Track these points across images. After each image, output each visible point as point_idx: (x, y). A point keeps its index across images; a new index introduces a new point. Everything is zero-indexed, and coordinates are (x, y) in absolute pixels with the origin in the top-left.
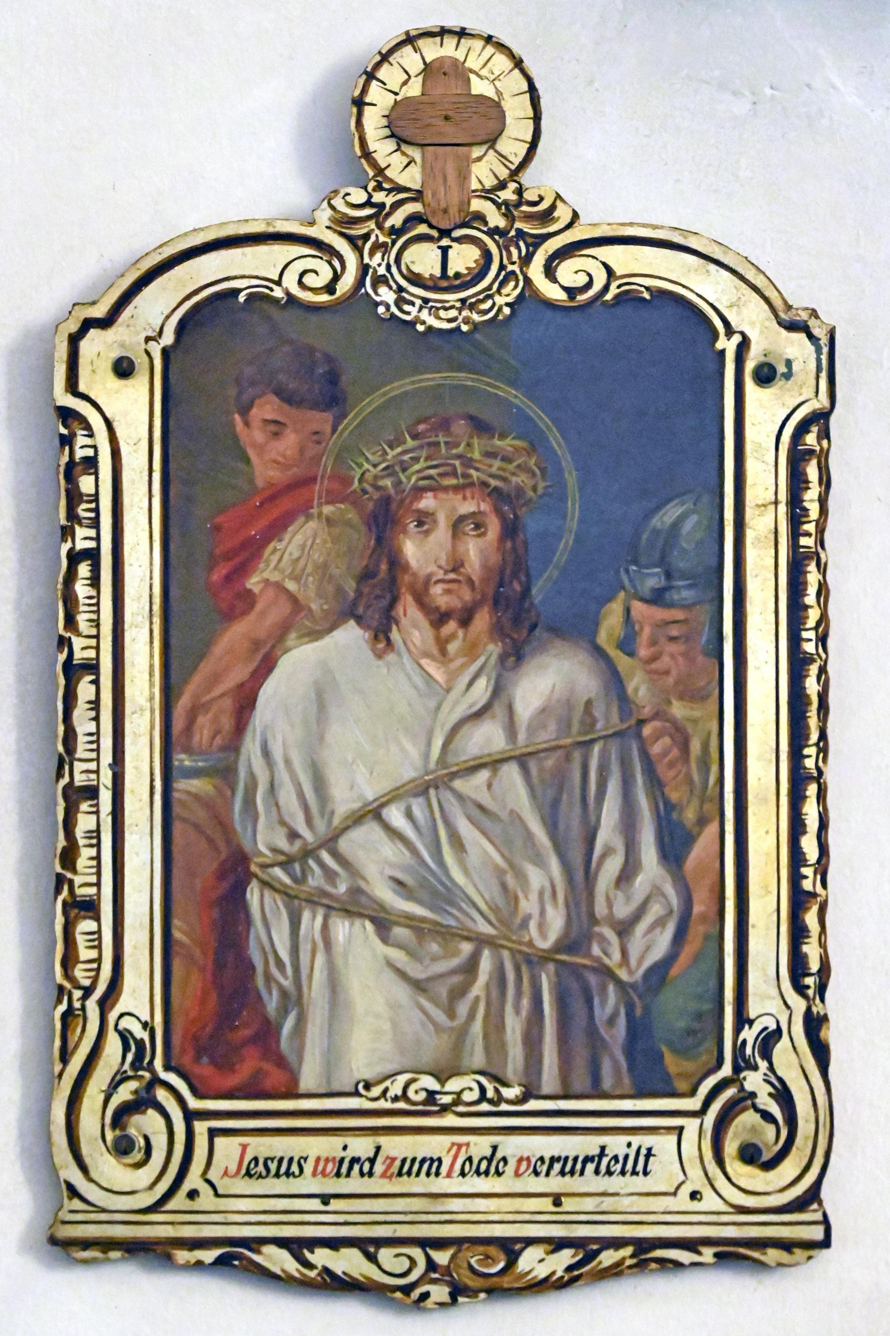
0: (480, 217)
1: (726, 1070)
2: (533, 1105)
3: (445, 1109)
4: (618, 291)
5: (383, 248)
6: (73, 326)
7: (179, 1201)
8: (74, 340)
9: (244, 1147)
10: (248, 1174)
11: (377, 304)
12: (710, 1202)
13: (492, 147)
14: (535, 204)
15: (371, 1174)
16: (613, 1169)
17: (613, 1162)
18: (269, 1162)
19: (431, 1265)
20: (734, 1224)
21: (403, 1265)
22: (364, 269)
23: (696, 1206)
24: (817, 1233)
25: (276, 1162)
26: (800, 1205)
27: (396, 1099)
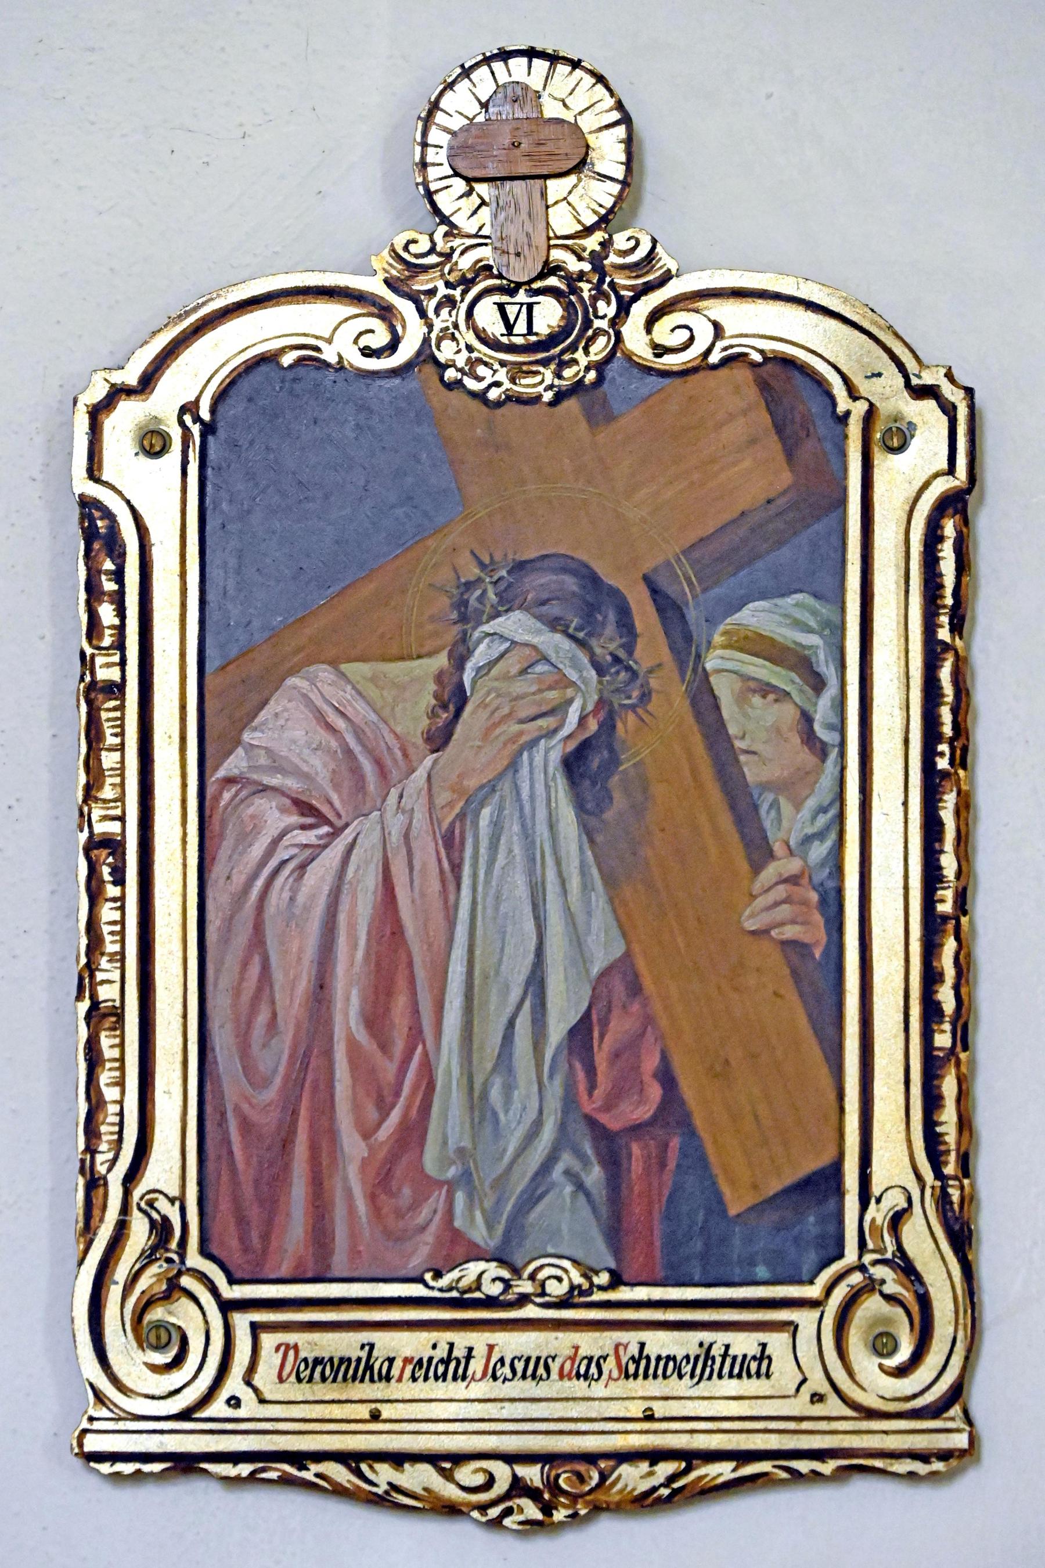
2: (624, 1294)
3: (523, 1300)
5: (450, 302)
6: (97, 392)
7: (218, 1408)
9: (491, 1348)
18: (516, 1361)
19: (516, 1479)
20: (641, 1432)
21: (480, 1479)
23: (818, 1410)
24: (961, 1441)
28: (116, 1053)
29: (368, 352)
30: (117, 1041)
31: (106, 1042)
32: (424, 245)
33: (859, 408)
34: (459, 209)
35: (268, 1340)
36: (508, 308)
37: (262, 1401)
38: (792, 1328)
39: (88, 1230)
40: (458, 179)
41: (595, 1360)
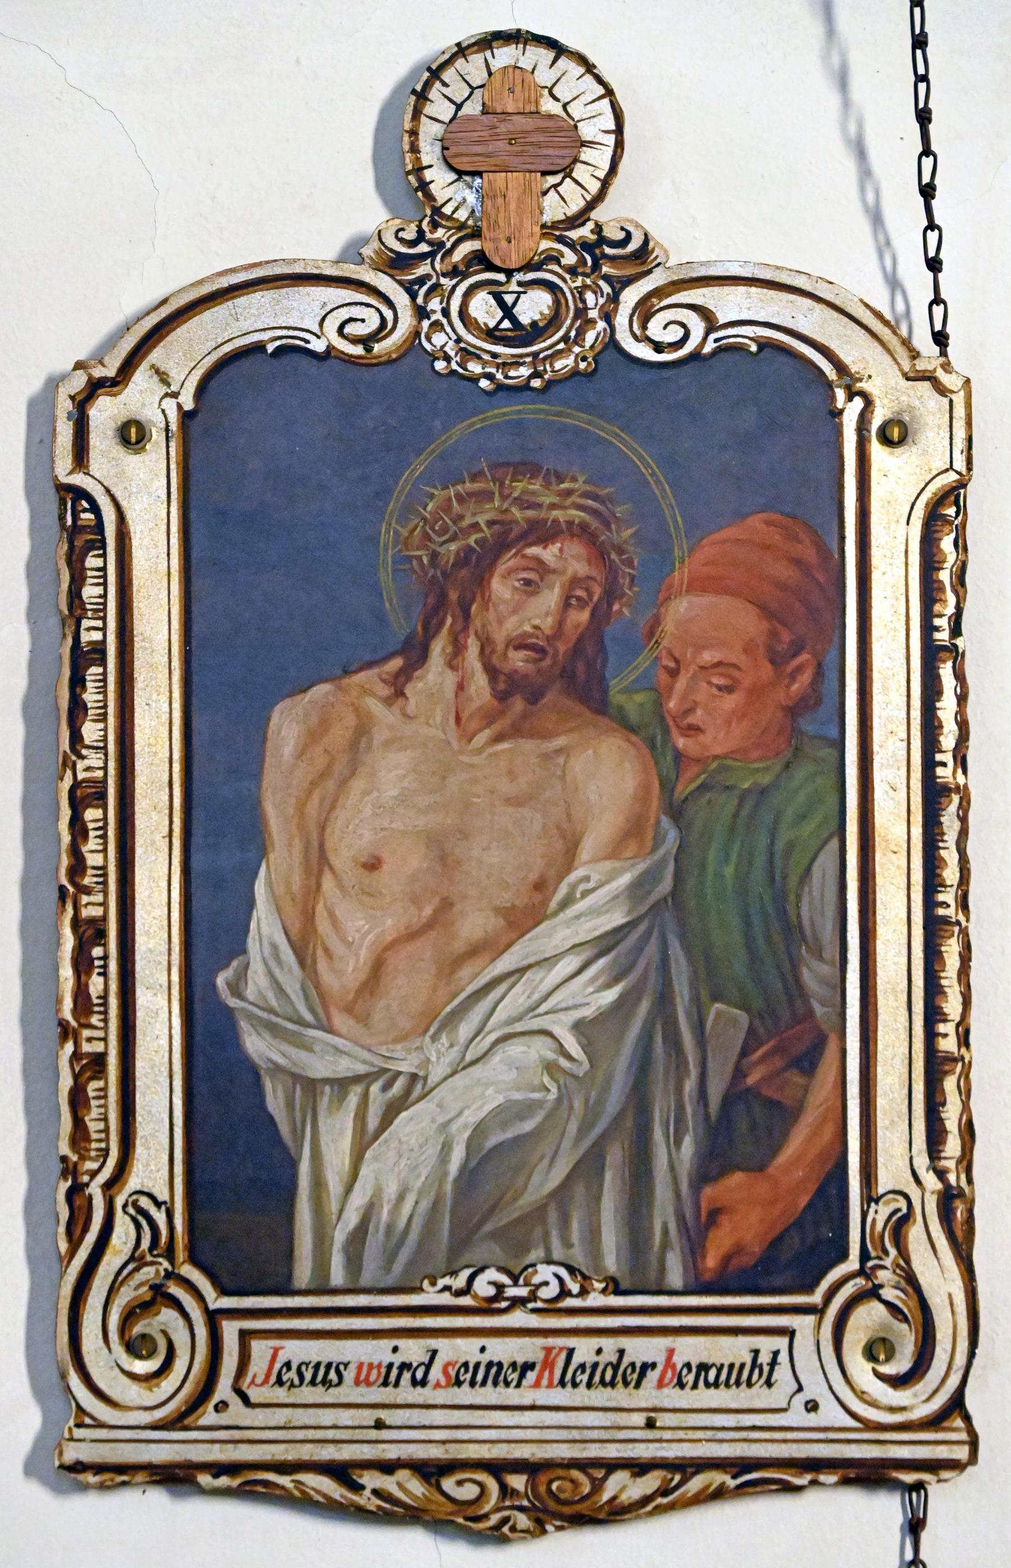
3: (518, 1302)
7: (209, 1416)
8: (82, 403)
10: (280, 1382)
13: (569, 175)
15: (423, 1383)
16: (462, 1378)
17: (462, 1370)
18: (304, 1368)
24: (962, 1453)
25: (311, 1371)
26: (935, 1422)
32: (410, 234)
35: (260, 1349)
41: (334, 1365)
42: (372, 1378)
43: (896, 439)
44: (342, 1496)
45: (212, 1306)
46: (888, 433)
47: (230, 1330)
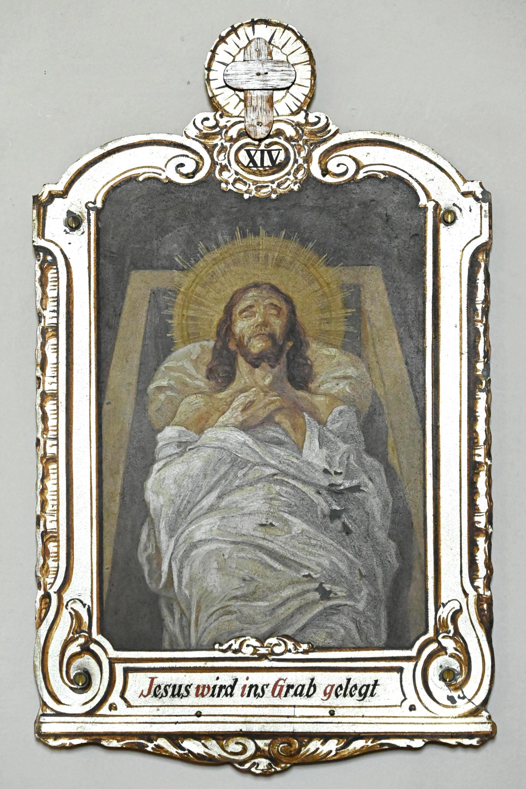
0: (280, 133)
1: (431, 633)
2: (312, 655)
4: (366, 174)
7: (105, 710)
9: (153, 679)
10: (155, 695)
11: (221, 182)
12: (420, 710)
14: (316, 124)
15: (231, 695)
16: (339, 694)
18: (167, 687)
19: (258, 748)
22: (214, 164)
23: (413, 713)
24: (487, 728)
27: (235, 651)
28: (55, 550)
29: (187, 176)
30: (56, 416)
31: (52, 546)
33: (431, 205)
34: (229, 103)
36: (273, 152)
37: (129, 705)
38: (400, 670)
39: (41, 620)
40: (227, 88)
42: (205, 693)
43: (449, 220)
44: (205, 752)
45: (110, 656)
46: (446, 219)
47: (119, 668)
